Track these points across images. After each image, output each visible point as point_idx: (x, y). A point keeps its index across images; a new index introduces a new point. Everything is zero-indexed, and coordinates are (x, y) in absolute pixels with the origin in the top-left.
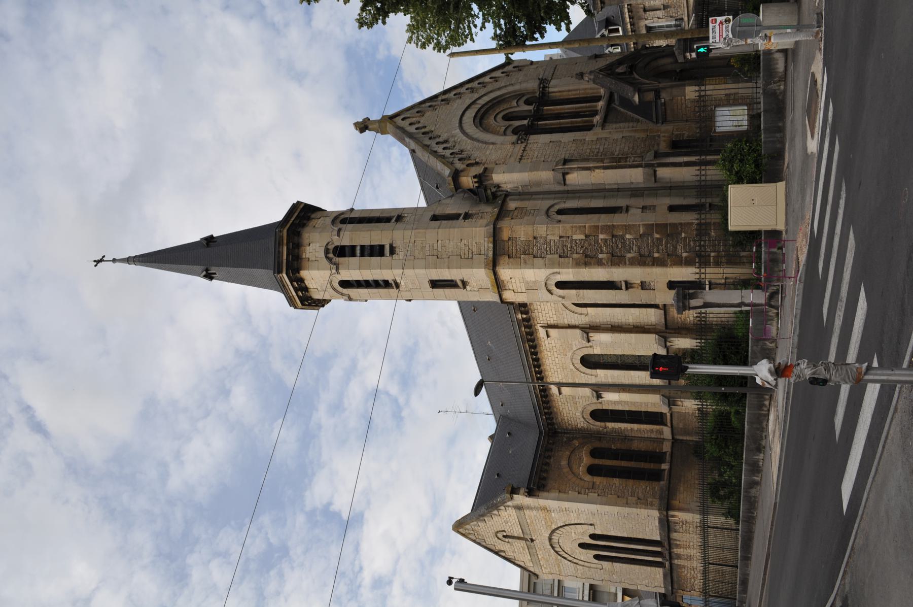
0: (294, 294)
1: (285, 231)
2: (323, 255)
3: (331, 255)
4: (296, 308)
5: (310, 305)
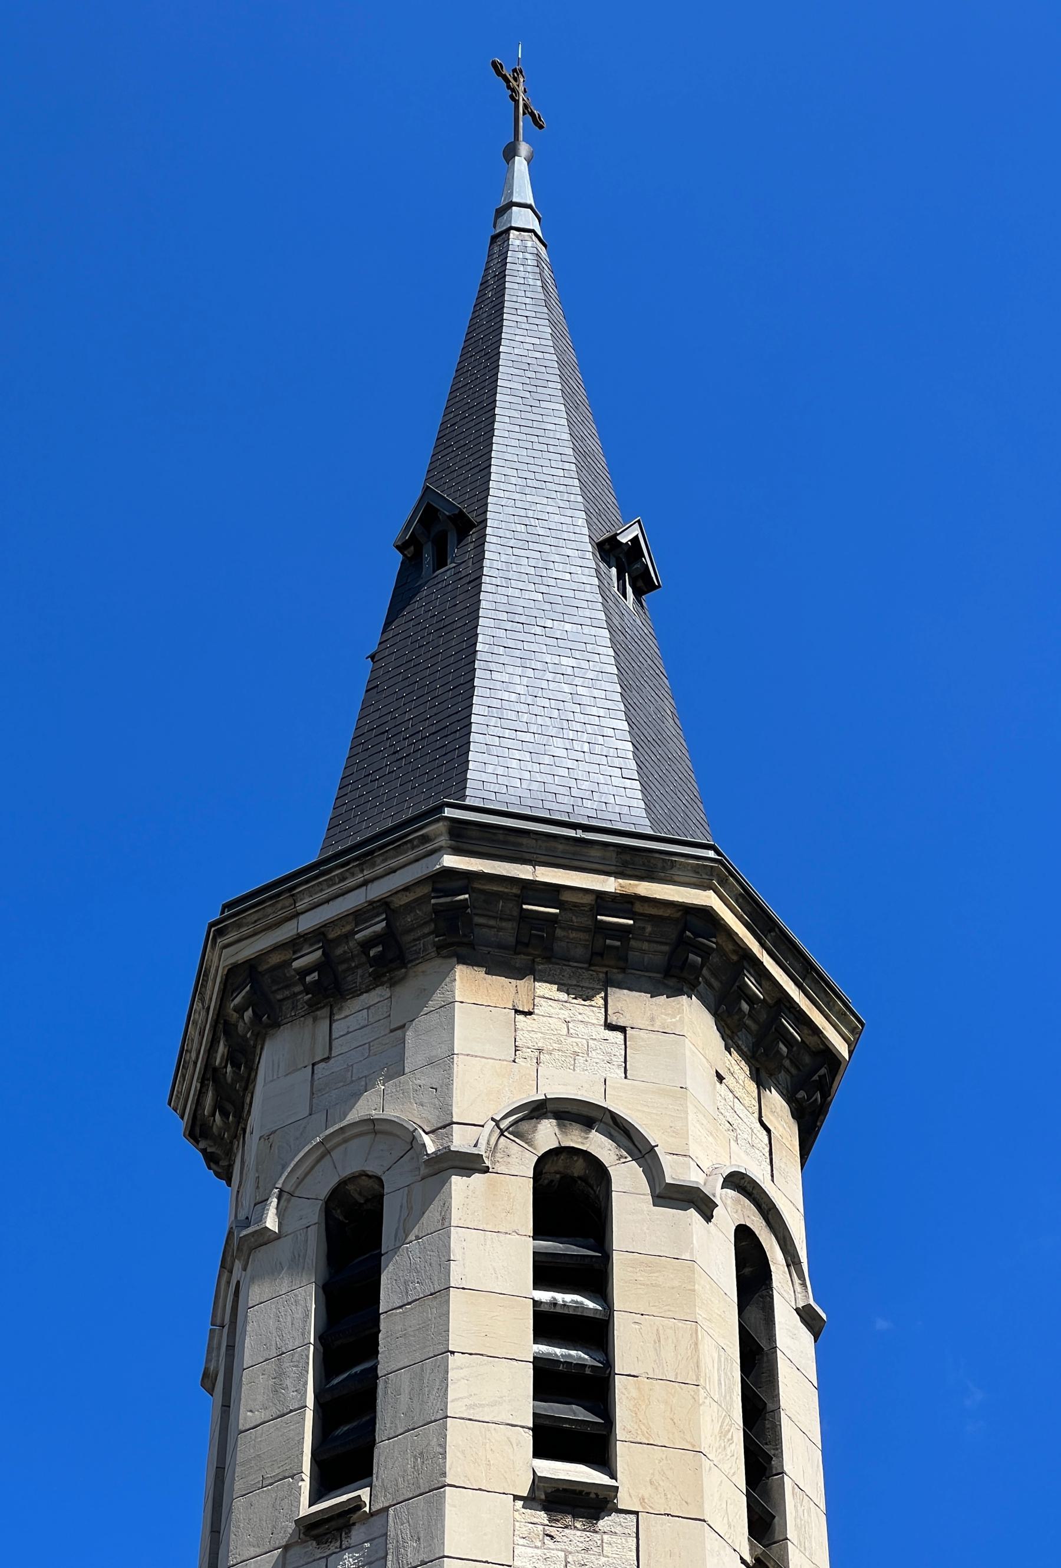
0: (307, 923)
1: (709, 899)
2: (558, 1085)
3: (548, 1135)
4: (218, 930)
5: (222, 1026)
